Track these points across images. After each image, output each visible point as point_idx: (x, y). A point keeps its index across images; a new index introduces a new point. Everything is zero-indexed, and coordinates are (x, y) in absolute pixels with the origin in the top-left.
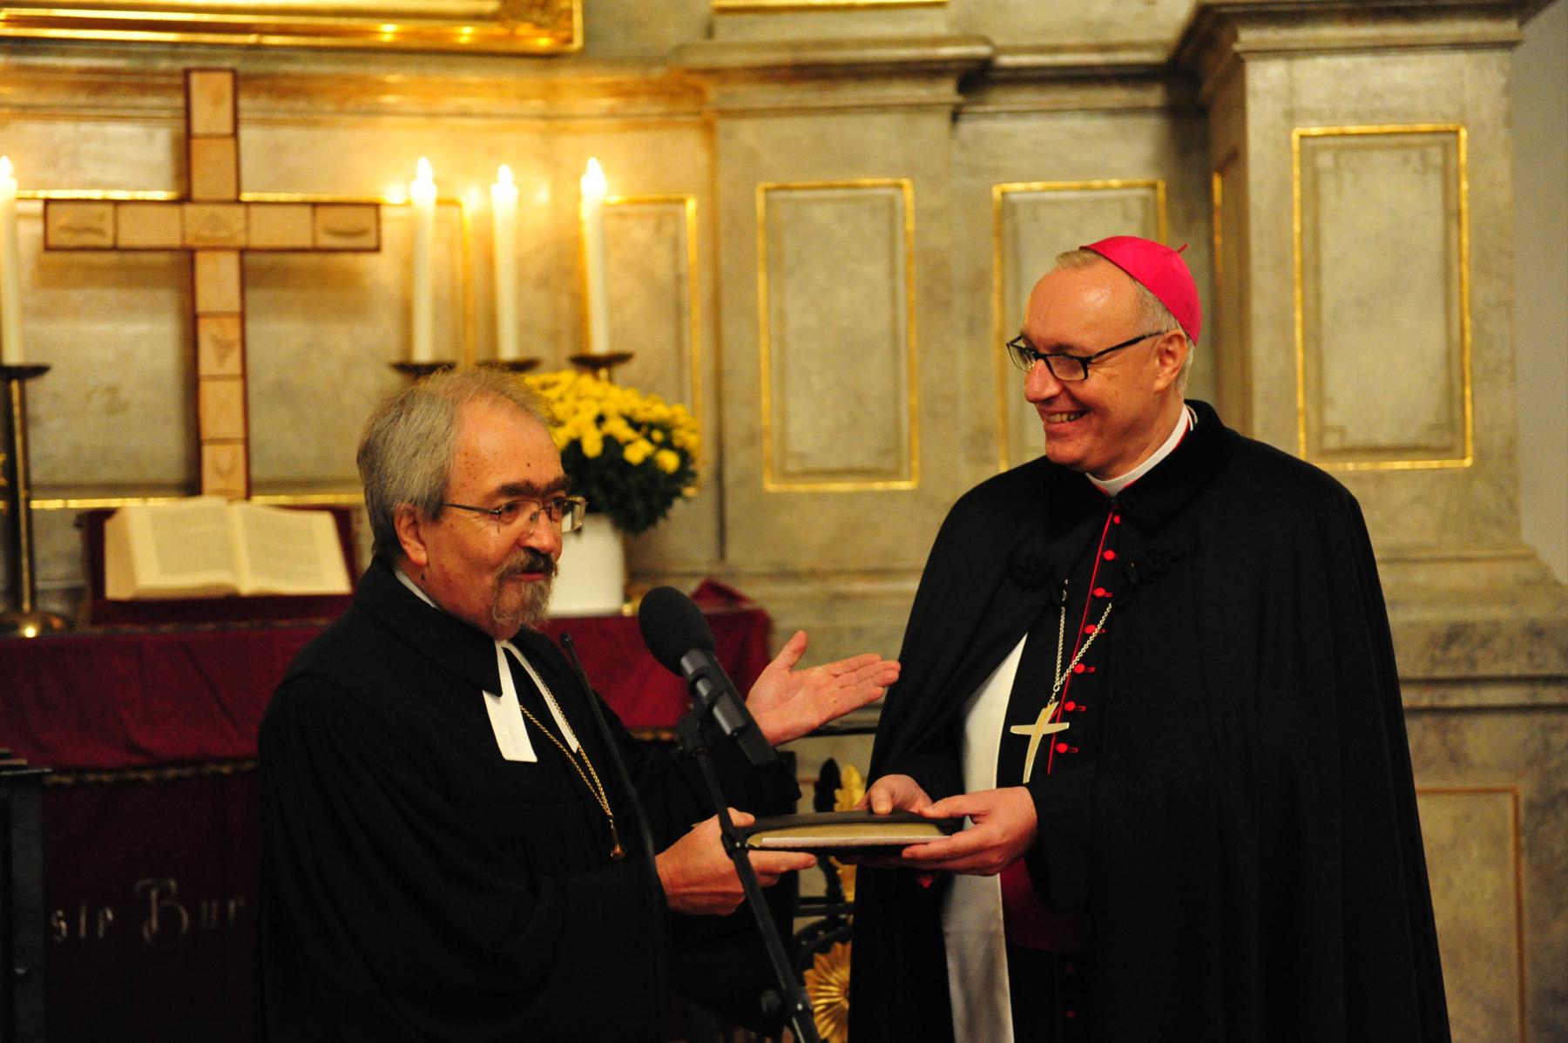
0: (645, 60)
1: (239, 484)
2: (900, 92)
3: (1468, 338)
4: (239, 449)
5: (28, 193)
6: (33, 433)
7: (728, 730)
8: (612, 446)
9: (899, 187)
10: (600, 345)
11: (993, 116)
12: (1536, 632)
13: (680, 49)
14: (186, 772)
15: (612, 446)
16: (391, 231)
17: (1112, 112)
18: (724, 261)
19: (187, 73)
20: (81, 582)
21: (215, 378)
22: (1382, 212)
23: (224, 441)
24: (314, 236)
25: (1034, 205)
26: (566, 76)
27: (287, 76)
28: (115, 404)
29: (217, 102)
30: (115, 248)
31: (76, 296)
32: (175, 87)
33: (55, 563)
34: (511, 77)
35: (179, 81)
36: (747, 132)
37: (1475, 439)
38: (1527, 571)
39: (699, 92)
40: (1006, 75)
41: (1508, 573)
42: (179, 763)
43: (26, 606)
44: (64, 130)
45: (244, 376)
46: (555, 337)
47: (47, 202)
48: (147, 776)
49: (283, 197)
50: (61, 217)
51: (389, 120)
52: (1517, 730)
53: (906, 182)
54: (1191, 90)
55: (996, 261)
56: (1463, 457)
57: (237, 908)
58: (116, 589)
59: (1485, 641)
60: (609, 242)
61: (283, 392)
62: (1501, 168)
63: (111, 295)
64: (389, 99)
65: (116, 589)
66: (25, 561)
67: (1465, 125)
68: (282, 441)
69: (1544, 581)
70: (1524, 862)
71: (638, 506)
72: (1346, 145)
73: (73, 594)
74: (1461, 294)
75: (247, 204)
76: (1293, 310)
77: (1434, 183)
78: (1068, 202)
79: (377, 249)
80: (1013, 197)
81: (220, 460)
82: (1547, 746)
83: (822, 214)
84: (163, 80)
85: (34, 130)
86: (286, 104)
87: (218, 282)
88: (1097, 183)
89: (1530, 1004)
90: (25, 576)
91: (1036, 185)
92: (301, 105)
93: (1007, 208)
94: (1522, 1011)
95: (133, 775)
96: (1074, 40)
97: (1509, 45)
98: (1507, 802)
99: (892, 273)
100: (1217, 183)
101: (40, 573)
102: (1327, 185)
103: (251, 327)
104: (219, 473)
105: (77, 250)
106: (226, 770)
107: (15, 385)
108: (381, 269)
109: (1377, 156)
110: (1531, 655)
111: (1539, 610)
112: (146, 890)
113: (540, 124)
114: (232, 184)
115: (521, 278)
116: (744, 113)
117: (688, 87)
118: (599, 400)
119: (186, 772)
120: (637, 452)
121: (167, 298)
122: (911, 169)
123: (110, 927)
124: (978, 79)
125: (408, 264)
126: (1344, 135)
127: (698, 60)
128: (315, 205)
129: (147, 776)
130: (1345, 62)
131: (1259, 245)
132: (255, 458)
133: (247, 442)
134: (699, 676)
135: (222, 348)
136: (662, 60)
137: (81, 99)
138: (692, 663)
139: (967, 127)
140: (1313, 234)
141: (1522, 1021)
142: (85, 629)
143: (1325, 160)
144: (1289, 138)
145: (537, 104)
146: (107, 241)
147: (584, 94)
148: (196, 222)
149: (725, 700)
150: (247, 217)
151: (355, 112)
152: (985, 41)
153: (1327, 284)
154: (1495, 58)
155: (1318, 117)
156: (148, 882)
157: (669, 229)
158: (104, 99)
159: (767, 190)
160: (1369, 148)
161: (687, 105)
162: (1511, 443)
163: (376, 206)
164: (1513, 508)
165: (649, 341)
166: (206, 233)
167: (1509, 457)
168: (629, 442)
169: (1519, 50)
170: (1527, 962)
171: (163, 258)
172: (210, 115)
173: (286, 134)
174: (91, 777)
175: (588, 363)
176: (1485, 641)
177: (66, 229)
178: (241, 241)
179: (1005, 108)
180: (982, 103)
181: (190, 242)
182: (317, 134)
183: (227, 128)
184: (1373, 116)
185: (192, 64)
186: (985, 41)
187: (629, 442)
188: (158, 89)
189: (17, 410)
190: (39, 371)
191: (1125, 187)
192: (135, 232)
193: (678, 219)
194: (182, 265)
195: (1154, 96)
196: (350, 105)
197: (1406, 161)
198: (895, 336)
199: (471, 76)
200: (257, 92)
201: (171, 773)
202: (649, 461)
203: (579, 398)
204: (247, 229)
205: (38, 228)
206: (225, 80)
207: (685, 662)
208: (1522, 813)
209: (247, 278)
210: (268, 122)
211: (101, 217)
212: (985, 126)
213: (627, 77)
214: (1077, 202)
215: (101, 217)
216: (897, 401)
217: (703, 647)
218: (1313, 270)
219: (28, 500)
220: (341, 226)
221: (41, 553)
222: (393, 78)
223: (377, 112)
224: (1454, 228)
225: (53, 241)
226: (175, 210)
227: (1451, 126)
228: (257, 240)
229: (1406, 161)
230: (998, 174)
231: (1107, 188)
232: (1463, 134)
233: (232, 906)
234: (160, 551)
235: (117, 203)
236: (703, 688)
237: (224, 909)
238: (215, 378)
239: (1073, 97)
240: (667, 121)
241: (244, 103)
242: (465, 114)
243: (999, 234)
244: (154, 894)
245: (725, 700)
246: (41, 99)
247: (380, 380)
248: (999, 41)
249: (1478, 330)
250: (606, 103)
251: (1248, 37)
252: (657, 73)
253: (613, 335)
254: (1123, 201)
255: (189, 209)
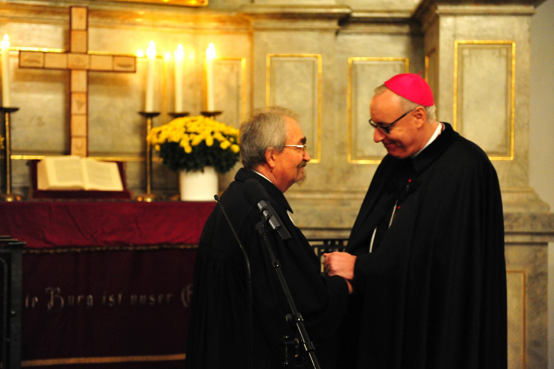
0: (229, 10)
1: (84, 152)
2: (318, 24)
3: (513, 115)
4: (84, 140)
5: (13, 48)
6: (13, 132)
7: (274, 228)
8: (217, 142)
9: (316, 57)
10: (211, 108)
11: (349, 34)
12: (534, 217)
13: (243, 6)
14: (65, 251)
15: (217, 142)
16: (140, 65)
17: (391, 34)
18: (255, 81)
19: (71, 8)
20: (28, 184)
21: (77, 115)
22: (485, 71)
23: (79, 137)
24: (113, 66)
25: (363, 66)
26: (202, 14)
27: (105, 11)
28: (40, 122)
29: (81, 18)
30: (43, 68)
31: (28, 84)
32: (66, 13)
33: (18, 178)
34: (182, 14)
35: (67, 11)
36: (264, 36)
37: (515, 150)
38: (531, 196)
39: (247, 22)
40: (355, 20)
41: (524, 197)
42: (62, 247)
43: (8, 192)
44: (26, 26)
45: (87, 114)
46: (195, 106)
47: (20, 51)
48: (51, 251)
49: (102, 52)
50: (25, 57)
51: (139, 28)
52: (525, 251)
53: (319, 56)
54: (419, 29)
55: (349, 84)
56: (510, 156)
57: (81, 299)
58: (41, 186)
59: (516, 220)
60: (216, 73)
61: (100, 121)
62: (526, 57)
63: (40, 85)
64: (138, 20)
65: (41, 186)
66: (8, 176)
67: (515, 41)
68: (100, 138)
69: (536, 200)
70: (527, 295)
71: (224, 164)
72: (473, 47)
73: (24, 189)
74: (511, 100)
75: (91, 55)
76: (453, 103)
77: (503, 61)
78: (375, 65)
79: (134, 72)
80: (356, 63)
81: (77, 143)
82: (536, 257)
83: (289, 66)
84: (60, 10)
85: (15, 26)
86: (104, 20)
87: (79, 81)
88: (385, 58)
89: (527, 346)
90: (8, 181)
91: (364, 59)
92: (109, 21)
93: (353, 67)
94: (524, 347)
95: (46, 251)
96: (379, 8)
97: (530, 14)
98: (521, 276)
99: (313, 87)
100: (427, 60)
101: (14, 180)
102: (467, 60)
103: (91, 98)
104: (77, 148)
105: (31, 69)
106: (79, 250)
107: (7, 115)
108: (135, 79)
109: (485, 52)
110: (532, 225)
111: (534, 209)
112: (49, 291)
113: (192, 31)
114: (85, 47)
115: (184, 85)
116: (264, 30)
117: (245, 21)
118: (212, 126)
119: (65, 251)
120: (225, 145)
121: (60, 87)
122: (321, 51)
123: (37, 304)
124: (345, 21)
125: (145, 78)
126: (473, 44)
127: (248, 10)
128: (114, 56)
129: (51, 251)
130: (474, 18)
131: (442, 80)
132: (90, 143)
133: (87, 137)
134: (264, 209)
135: (80, 104)
136: (235, 10)
137: (32, 16)
138: (262, 205)
139: (341, 38)
140: (461, 78)
141: (524, 352)
142: (31, 199)
143: (466, 52)
144: (454, 43)
145: (191, 24)
146: (41, 65)
147: (208, 21)
148: (72, 60)
149: (273, 217)
150: (90, 59)
151: (128, 24)
152: (348, 7)
153: (466, 96)
154: (525, 19)
155: (463, 37)
156: (49, 288)
157: (236, 69)
158: (40, 16)
159: (271, 57)
160: (481, 49)
161: (243, 26)
162: (527, 152)
163: (135, 58)
164: (526, 174)
165: (227, 108)
166: (75, 63)
167: (526, 157)
168: (222, 141)
169: (534, 17)
170: (527, 331)
171: (59, 72)
172: (78, 22)
173: (105, 31)
174: (32, 251)
175: (207, 114)
176: (516, 220)
177: (27, 60)
178: (87, 67)
179: (354, 31)
180: (346, 29)
181: (70, 67)
182: (115, 31)
183: (84, 27)
184: (483, 37)
185: (72, 4)
186: (348, 7)
187: (222, 141)
188: (59, 13)
189: (7, 123)
190: (15, 110)
191: (395, 60)
192: (50, 63)
193: (239, 66)
194: (66, 75)
195: (406, 29)
196: (126, 22)
197: (494, 53)
198: (313, 109)
199: (168, 13)
200: (94, 16)
201: (59, 251)
202: (229, 149)
203: (206, 125)
204: (90, 63)
205: (17, 60)
206: (83, 11)
207: (259, 205)
208: (527, 281)
209: (89, 81)
210: (97, 26)
211: (39, 57)
212: (347, 37)
213: (223, 15)
214: (378, 65)
215: (39, 57)
216: (313, 131)
217: (265, 200)
218: (461, 90)
219: (10, 155)
220: (122, 63)
221: (14, 174)
222: (141, 12)
223: (135, 24)
224: (509, 76)
225: (22, 64)
226: (65, 56)
227: (509, 42)
228: (94, 66)
229: (494, 53)
230: (351, 54)
231: (388, 61)
232: (514, 45)
233: (79, 298)
234: (59, 174)
235: (45, 53)
236: (265, 214)
237: (76, 299)
238: (77, 115)
239: (377, 28)
240: (236, 32)
241: (90, 19)
242: (166, 26)
243: (350, 75)
244: (52, 293)
245: (273, 217)
246: (18, 15)
247: (138, 118)
248: (354, 8)
249: (517, 113)
250: (215, 24)
251: (441, 8)
252: (234, 14)
253: (216, 105)
254: (394, 65)
255: (70, 55)
